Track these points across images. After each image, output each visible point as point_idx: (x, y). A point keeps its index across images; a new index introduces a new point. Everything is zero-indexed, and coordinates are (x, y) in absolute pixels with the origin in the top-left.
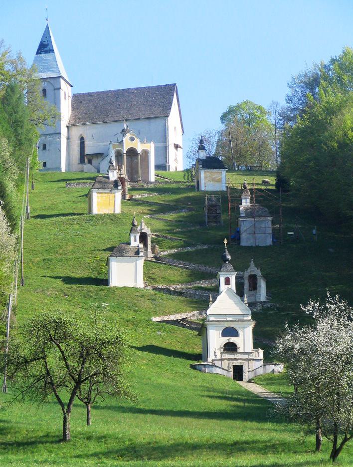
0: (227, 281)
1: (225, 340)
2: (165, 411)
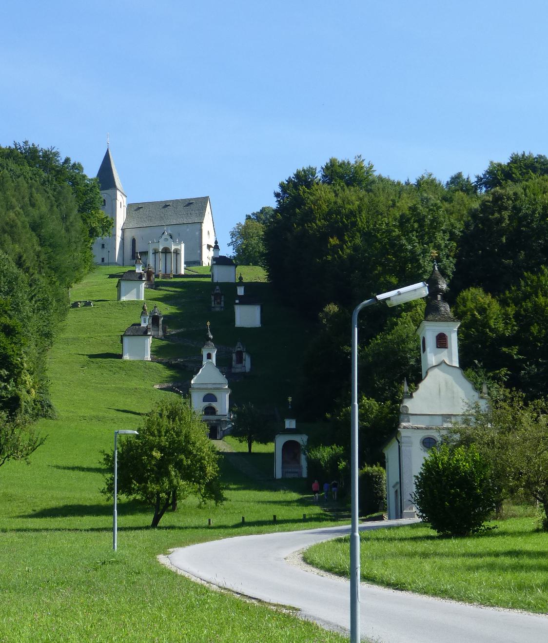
0: (209, 356)
1: (206, 404)
2: (248, 526)
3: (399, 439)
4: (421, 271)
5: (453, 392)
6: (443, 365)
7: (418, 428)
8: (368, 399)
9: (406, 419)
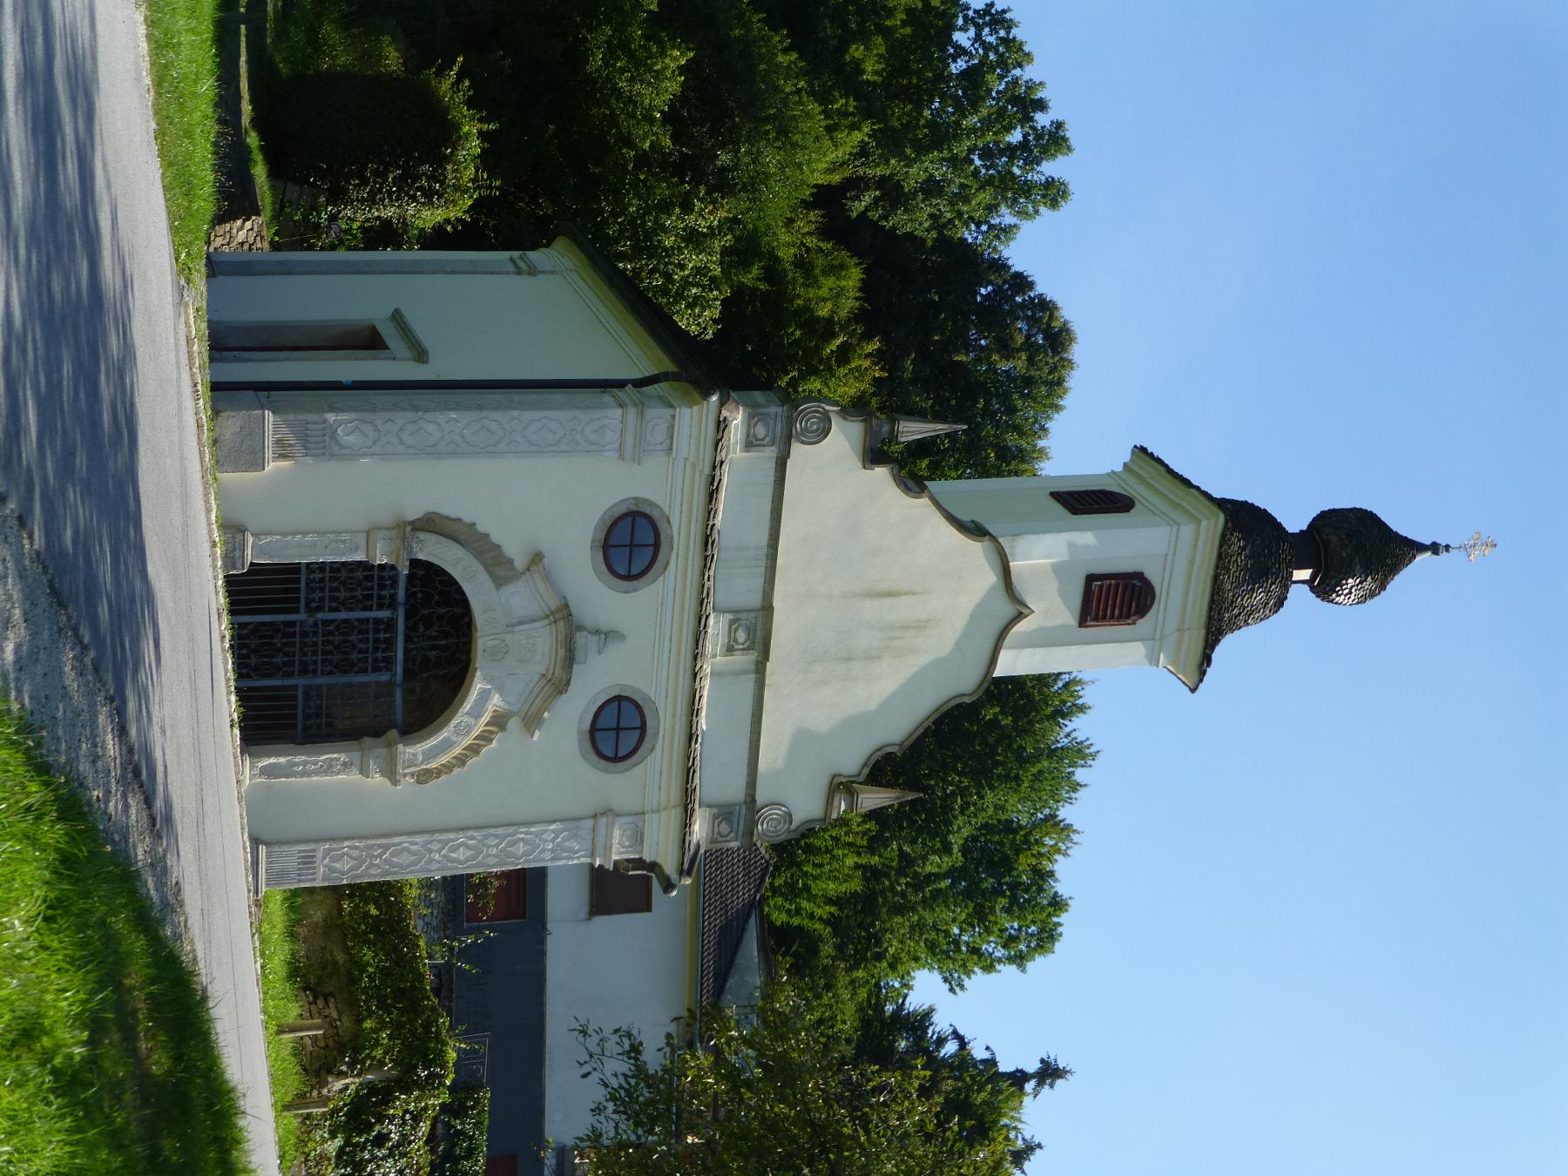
3: (662, 388)
4: (908, 151)
5: (872, 657)
6: (1008, 610)
7: (712, 495)
8: (683, 70)
9: (760, 430)
